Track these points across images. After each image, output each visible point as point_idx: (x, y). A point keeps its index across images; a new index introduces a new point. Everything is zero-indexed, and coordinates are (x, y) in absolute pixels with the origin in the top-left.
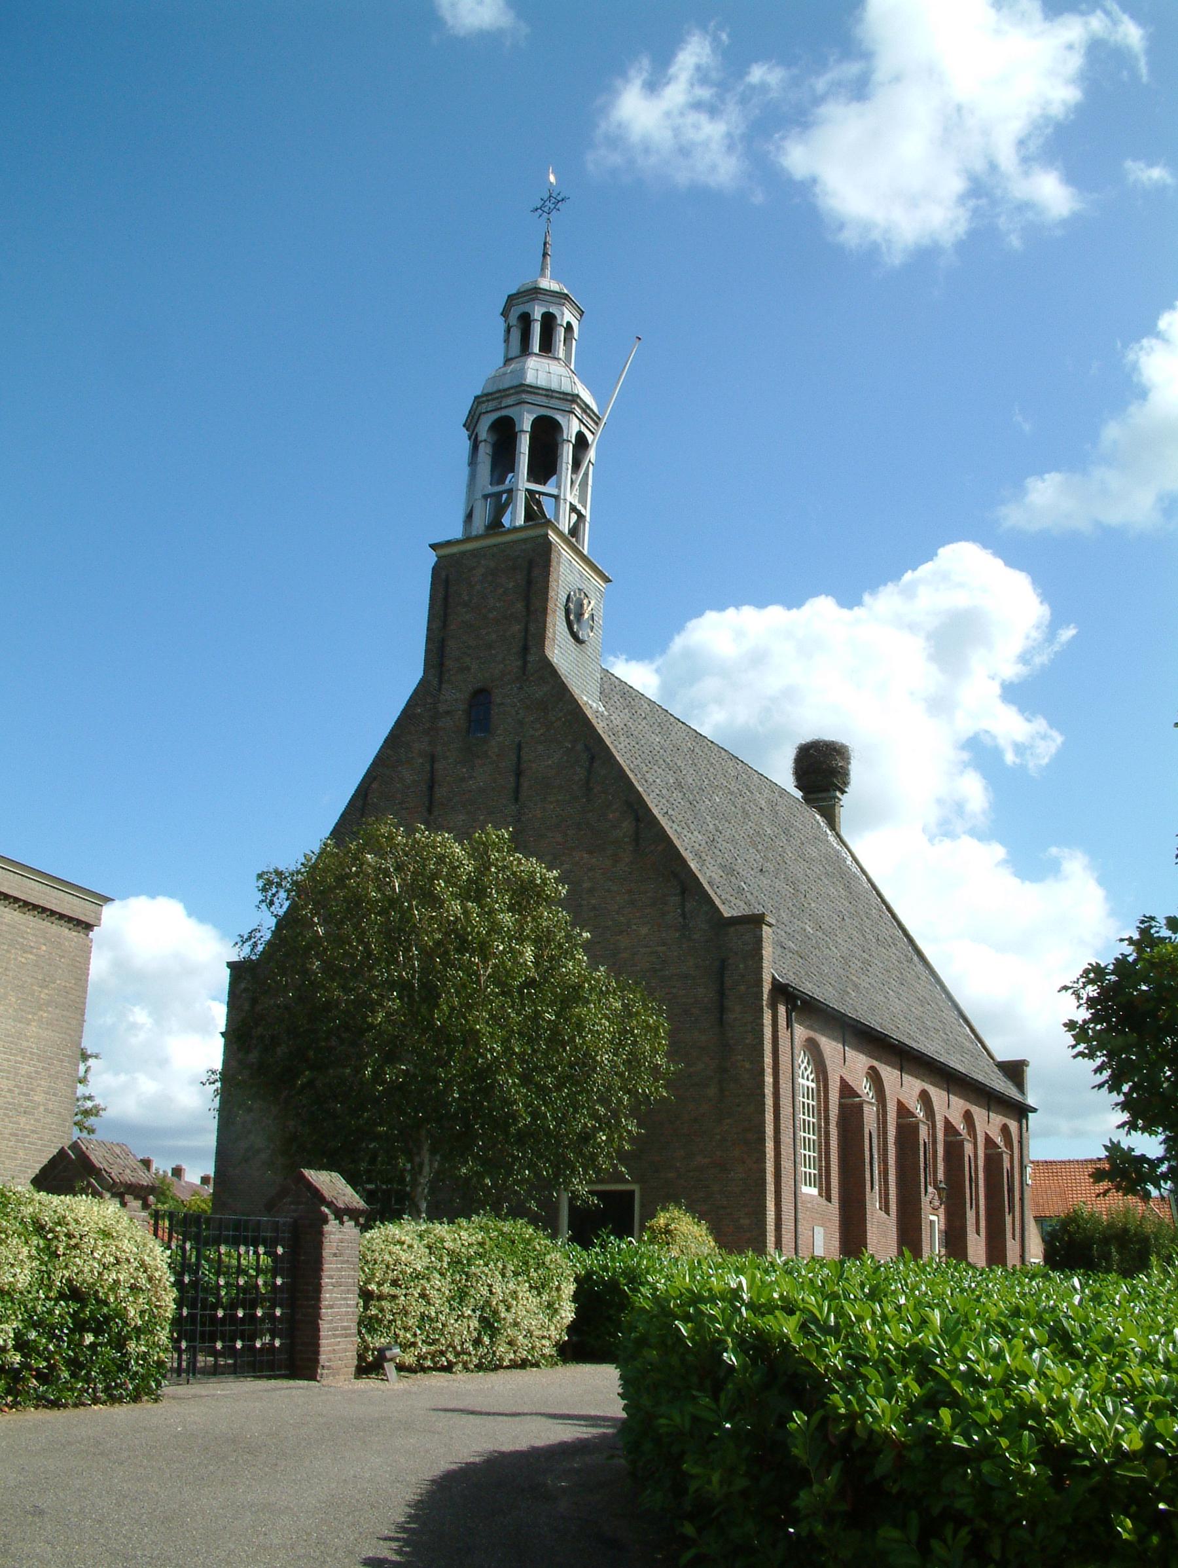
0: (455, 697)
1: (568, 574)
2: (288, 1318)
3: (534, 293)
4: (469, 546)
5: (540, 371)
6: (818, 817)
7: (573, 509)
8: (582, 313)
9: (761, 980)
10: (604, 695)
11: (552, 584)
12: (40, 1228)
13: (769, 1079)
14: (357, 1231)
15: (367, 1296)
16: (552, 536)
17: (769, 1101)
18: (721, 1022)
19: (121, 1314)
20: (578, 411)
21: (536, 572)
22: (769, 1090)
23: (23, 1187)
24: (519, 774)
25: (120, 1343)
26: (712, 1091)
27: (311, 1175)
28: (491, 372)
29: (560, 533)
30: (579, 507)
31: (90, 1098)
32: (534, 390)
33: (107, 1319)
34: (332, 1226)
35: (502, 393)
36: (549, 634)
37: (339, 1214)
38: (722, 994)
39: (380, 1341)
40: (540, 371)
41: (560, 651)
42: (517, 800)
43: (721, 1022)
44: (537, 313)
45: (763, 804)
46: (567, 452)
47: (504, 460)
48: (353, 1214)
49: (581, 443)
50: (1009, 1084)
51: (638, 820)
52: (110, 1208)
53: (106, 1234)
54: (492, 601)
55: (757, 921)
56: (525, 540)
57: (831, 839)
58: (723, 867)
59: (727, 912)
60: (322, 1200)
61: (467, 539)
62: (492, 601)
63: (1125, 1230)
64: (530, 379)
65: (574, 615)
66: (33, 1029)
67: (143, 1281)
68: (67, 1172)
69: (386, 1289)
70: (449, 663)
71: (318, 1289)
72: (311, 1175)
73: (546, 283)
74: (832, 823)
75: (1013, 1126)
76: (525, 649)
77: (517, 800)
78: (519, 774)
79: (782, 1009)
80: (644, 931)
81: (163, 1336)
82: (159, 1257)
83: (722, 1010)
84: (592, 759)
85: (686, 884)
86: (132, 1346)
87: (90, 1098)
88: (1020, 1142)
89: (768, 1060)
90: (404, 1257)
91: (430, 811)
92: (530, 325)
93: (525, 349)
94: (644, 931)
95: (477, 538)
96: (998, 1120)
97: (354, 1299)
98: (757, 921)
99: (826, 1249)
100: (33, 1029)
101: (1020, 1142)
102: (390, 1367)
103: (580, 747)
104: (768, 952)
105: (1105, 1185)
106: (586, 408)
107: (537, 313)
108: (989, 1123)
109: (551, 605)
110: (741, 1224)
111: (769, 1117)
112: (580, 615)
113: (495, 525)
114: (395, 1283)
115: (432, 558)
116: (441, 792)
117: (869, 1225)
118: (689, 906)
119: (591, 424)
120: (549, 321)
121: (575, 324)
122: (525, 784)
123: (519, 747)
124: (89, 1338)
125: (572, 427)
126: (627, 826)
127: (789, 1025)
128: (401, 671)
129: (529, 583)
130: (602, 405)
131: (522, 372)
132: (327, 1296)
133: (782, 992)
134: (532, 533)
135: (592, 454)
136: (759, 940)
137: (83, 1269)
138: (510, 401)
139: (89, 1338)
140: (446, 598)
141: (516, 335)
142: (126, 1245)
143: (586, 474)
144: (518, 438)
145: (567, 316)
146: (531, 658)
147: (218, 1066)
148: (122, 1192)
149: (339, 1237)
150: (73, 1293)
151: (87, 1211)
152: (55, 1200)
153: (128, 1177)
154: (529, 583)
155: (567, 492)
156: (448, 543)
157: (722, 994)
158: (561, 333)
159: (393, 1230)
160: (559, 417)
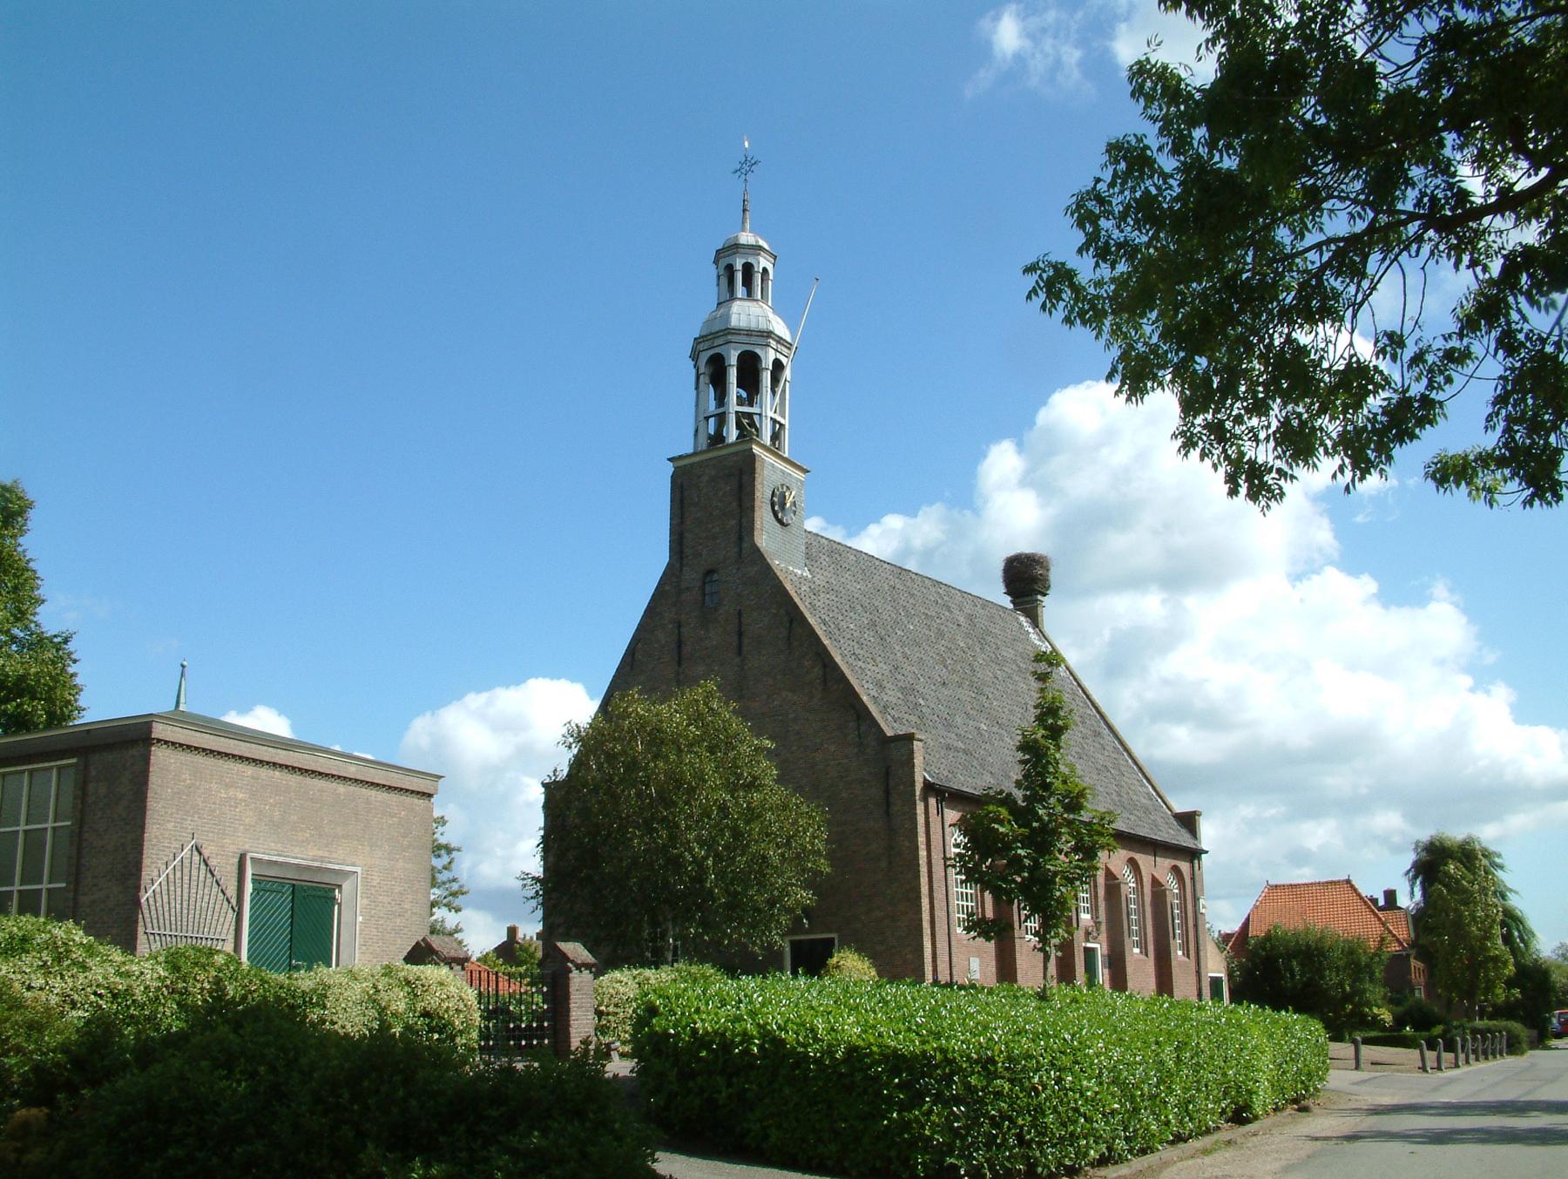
0: (691, 576)
1: (770, 471)
2: (553, 1027)
3: (734, 247)
4: (697, 459)
5: (744, 313)
6: (1022, 619)
7: (774, 421)
8: (775, 258)
9: (913, 782)
10: (810, 558)
11: (758, 486)
12: (408, 983)
13: (923, 853)
14: (591, 976)
15: (599, 1014)
16: (756, 450)
17: (924, 869)
18: (888, 813)
19: (453, 1024)
20: (773, 343)
21: (745, 478)
22: (923, 861)
23: (400, 963)
24: (740, 634)
25: (452, 1038)
26: (883, 864)
27: (562, 945)
28: (705, 317)
29: (763, 447)
30: (779, 418)
31: (454, 880)
32: (737, 331)
33: (445, 1026)
34: (575, 974)
35: (715, 335)
36: (758, 525)
37: (578, 967)
38: (887, 792)
39: (607, 1040)
40: (744, 313)
41: (766, 536)
42: (740, 653)
43: (888, 813)
44: (739, 266)
45: (961, 619)
46: (766, 378)
47: (718, 379)
48: (588, 966)
49: (778, 366)
50: (1183, 831)
51: (825, 666)
52: (445, 970)
53: (441, 984)
54: (715, 496)
55: (909, 738)
56: (736, 454)
57: (1033, 637)
58: (902, 689)
59: (889, 733)
60: (568, 959)
61: (695, 454)
62: (715, 496)
63: (1308, 946)
64: (734, 323)
65: (778, 504)
66: (401, 864)
67: (462, 1007)
68: (421, 954)
69: (611, 1009)
70: (688, 551)
71: (568, 1010)
72: (562, 945)
73: (746, 238)
74: (1035, 622)
75: (1184, 866)
76: (740, 539)
77: (740, 653)
78: (740, 634)
79: (932, 801)
80: (832, 748)
81: (475, 1035)
82: (471, 994)
83: (888, 804)
84: (791, 622)
85: (862, 713)
86: (458, 1040)
87: (454, 880)
88: (1193, 879)
89: (922, 839)
90: (622, 990)
91: (679, 663)
92: (736, 272)
93: (732, 297)
94: (832, 748)
95: (702, 452)
96: (1165, 863)
97: (591, 1015)
98: (909, 738)
99: (983, 972)
100: (401, 864)
101: (1193, 879)
102: (615, 1055)
103: (782, 612)
104: (918, 760)
105: (973, 934)
106: (780, 340)
107: (739, 266)
108: (1158, 868)
109: (757, 503)
110: (899, 957)
111: (924, 880)
112: (783, 505)
113: (718, 439)
114: (616, 1006)
115: (670, 469)
116: (687, 649)
117: (1018, 956)
118: (863, 728)
119: (785, 351)
120: (748, 269)
121: (770, 268)
122: (746, 641)
123: (740, 614)
124: (436, 1036)
125: (769, 357)
126: (817, 671)
127: (940, 813)
128: (654, 557)
129: (741, 486)
130: (793, 335)
131: (727, 317)
132: (574, 1014)
133: (929, 788)
134: (740, 448)
135: (787, 373)
136: (912, 752)
137: (431, 1002)
138: (720, 341)
139: (436, 1036)
140: (682, 501)
141: (724, 281)
142: (452, 988)
143: (784, 391)
144: (730, 366)
145: (763, 262)
146: (745, 545)
147: (536, 867)
148: (450, 962)
149: (580, 981)
150: (426, 1014)
151: (431, 973)
152: (415, 968)
153: (453, 954)
154: (741, 486)
155: (767, 407)
156: (681, 457)
157: (887, 792)
158: (758, 279)
159: (617, 974)
160: (758, 351)
